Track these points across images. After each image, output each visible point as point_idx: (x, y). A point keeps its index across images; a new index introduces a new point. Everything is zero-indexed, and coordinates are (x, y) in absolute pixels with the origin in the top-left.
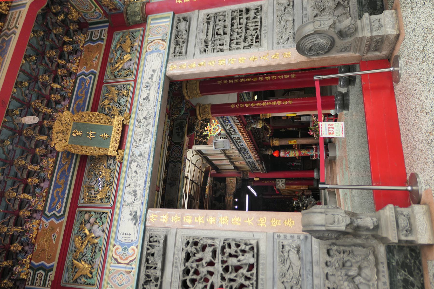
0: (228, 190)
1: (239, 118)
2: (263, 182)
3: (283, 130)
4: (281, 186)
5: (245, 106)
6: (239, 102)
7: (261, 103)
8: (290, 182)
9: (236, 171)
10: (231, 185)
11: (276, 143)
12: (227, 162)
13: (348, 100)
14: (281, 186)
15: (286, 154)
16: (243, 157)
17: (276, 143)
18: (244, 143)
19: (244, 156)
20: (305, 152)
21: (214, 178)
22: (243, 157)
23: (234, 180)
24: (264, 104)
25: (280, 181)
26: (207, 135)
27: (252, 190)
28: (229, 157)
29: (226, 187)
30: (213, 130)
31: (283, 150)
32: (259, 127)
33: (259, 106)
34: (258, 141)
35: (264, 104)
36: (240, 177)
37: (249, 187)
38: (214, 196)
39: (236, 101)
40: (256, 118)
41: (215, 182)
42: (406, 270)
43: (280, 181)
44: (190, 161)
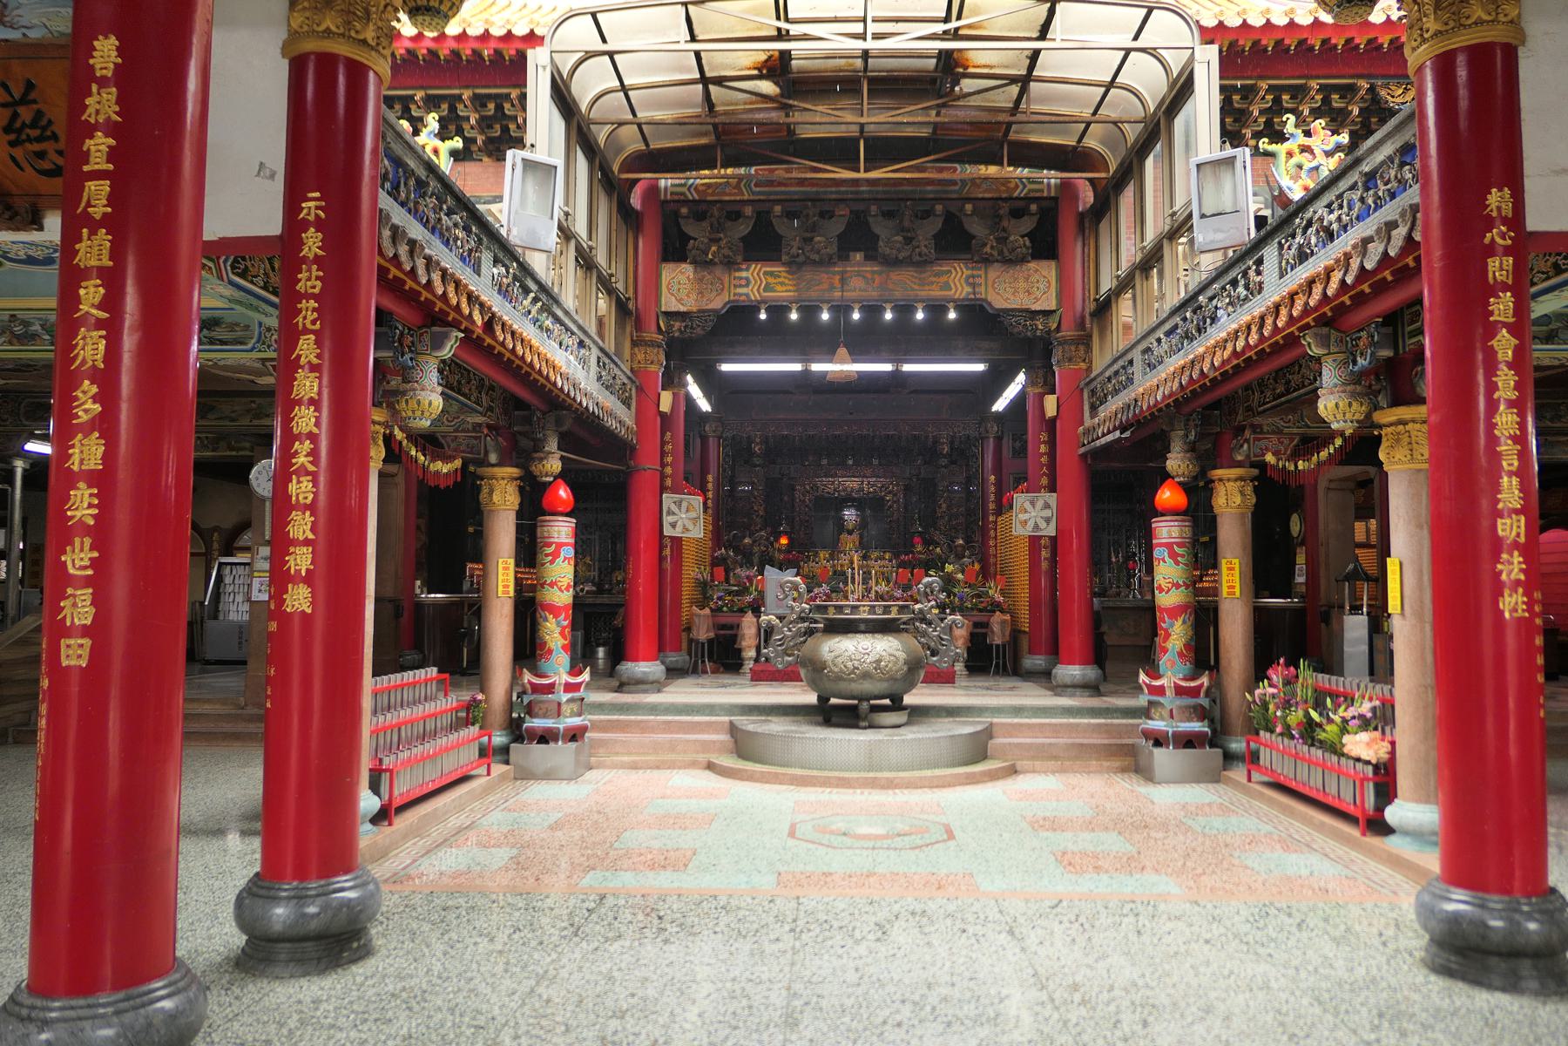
0: (994, 272)
1: (1402, 268)
2: (1044, 437)
3: (1295, 526)
4: (1022, 517)
5: (1493, 290)
6: (1524, 243)
7: (1517, 405)
8: (1044, 554)
9: (1093, 306)
10: (1022, 284)
11: (1231, 499)
12: (1130, 253)
13: (1512, 986)
14: (1022, 517)
15: (1169, 546)
16: (1153, 330)
18: (1227, 323)
19: (1160, 334)
20: (1176, 635)
21: (1055, 199)
22: (1153, 330)
24: (1506, 420)
25: (1048, 513)
26: (1280, 137)
28: (1151, 261)
30: (1307, 165)
31: (1188, 532)
32: (1321, 405)
33: (1492, 388)
34: (1241, 401)
35: (1506, 420)
36: (1058, 329)
38: (969, 207)
39: (1533, 223)
40: (1393, 381)
41: (1034, 207)
42: (1127, 434)
43: (1048, 513)
44: (1128, 51)
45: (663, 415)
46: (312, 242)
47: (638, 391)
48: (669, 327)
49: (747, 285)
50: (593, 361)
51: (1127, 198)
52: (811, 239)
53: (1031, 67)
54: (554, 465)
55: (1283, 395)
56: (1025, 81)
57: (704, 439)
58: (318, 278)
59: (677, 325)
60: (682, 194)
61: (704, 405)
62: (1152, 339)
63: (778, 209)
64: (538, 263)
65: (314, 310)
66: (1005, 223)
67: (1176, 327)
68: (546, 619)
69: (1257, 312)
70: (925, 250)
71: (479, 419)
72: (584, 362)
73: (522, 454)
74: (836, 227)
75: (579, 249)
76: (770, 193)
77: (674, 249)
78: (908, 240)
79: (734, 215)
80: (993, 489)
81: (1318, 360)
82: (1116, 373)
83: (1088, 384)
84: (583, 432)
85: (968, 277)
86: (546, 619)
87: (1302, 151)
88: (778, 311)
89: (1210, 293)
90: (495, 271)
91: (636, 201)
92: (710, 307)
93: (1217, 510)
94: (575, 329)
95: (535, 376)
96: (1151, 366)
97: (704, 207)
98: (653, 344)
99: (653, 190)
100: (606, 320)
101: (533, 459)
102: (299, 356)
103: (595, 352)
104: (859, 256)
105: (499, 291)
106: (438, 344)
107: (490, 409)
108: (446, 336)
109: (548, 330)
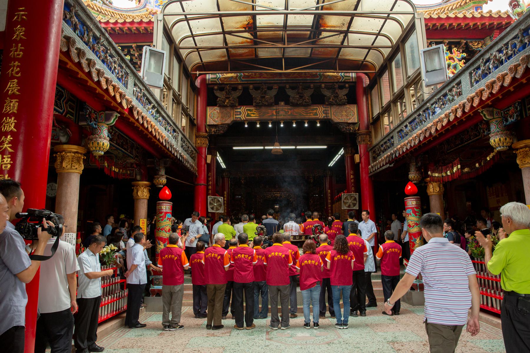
10: (344, 113)
12: (387, 98)
15: (412, 208)
17: (433, 189)
19: (407, 123)
21: (355, 82)
23: (354, 119)
27: (337, 158)
28: (400, 97)
29: (341, 104)
36: (359, 129)
37: (342, 152)
41: (347, 85)
42: (392, 165)
45: (208, 164)
46: (20, 32)
47: (196, 153)
48: (210, 130)
49: (240, 114)
50: (180, 138)
51: (386, 77)
52: (264, 97)
53: (349, 27)
54: (164, 180)
55: (460, 144)
56: (346, 33)
57: (223, 178)
58: (21, 50)
59: (213, 130)
60: (215, 81)
61: (223, 166)
62: (403, 126)
63: (251, 86)
64: (157, 93)
65: (18, 66)
66: (337, 91)
67: (415, 119)
68: (160, 244)
69: (454, 108)
70: (307, 100)
71: (132, 161)
72: (176, 138)
73: (150, 176)
74: (273, 93)
75: (174, 95)
76: (248, 81)
77: (211, 101)
78: (301, 97)
79: (235, 89)
80: (329, 195)
81: (488, 124)
82: (385, 143)
83: (371, 150)
84: (175, 166)
85: (324, 111)
86: (160, 244)
87: (449, 59)
88: (252, 123)
89: (432, 102)
90: (135, 89)
91: (198, 83)
92: (226, 122)
93: (429, 194)
94: (172, 124)
95: (154, 140)
96: (402, 137)
97: (223, 86)
98: (204, 137)
99: (204, 80)
100: (185, 128)
101: (155, 178)
102: (8, 91)
103: (180, 136)
104: (282, 103)
105: (137, 99)
106: (108, 118)
107: (137, 156)
108: (111, 115)
109: (160, 121)
